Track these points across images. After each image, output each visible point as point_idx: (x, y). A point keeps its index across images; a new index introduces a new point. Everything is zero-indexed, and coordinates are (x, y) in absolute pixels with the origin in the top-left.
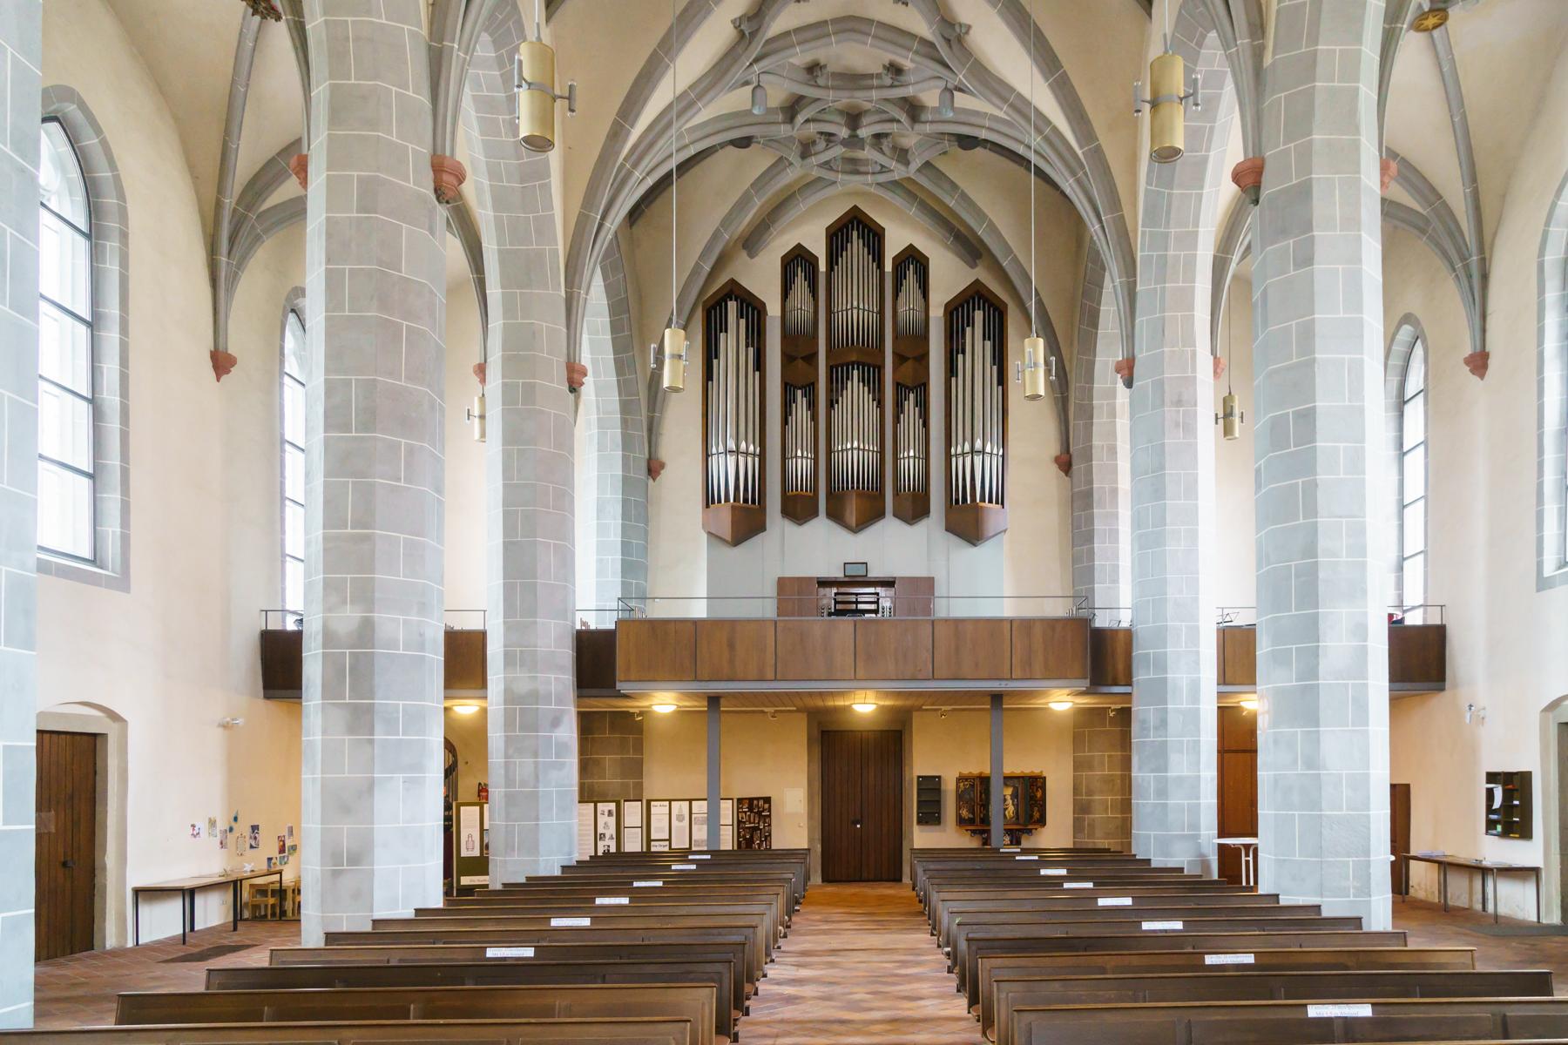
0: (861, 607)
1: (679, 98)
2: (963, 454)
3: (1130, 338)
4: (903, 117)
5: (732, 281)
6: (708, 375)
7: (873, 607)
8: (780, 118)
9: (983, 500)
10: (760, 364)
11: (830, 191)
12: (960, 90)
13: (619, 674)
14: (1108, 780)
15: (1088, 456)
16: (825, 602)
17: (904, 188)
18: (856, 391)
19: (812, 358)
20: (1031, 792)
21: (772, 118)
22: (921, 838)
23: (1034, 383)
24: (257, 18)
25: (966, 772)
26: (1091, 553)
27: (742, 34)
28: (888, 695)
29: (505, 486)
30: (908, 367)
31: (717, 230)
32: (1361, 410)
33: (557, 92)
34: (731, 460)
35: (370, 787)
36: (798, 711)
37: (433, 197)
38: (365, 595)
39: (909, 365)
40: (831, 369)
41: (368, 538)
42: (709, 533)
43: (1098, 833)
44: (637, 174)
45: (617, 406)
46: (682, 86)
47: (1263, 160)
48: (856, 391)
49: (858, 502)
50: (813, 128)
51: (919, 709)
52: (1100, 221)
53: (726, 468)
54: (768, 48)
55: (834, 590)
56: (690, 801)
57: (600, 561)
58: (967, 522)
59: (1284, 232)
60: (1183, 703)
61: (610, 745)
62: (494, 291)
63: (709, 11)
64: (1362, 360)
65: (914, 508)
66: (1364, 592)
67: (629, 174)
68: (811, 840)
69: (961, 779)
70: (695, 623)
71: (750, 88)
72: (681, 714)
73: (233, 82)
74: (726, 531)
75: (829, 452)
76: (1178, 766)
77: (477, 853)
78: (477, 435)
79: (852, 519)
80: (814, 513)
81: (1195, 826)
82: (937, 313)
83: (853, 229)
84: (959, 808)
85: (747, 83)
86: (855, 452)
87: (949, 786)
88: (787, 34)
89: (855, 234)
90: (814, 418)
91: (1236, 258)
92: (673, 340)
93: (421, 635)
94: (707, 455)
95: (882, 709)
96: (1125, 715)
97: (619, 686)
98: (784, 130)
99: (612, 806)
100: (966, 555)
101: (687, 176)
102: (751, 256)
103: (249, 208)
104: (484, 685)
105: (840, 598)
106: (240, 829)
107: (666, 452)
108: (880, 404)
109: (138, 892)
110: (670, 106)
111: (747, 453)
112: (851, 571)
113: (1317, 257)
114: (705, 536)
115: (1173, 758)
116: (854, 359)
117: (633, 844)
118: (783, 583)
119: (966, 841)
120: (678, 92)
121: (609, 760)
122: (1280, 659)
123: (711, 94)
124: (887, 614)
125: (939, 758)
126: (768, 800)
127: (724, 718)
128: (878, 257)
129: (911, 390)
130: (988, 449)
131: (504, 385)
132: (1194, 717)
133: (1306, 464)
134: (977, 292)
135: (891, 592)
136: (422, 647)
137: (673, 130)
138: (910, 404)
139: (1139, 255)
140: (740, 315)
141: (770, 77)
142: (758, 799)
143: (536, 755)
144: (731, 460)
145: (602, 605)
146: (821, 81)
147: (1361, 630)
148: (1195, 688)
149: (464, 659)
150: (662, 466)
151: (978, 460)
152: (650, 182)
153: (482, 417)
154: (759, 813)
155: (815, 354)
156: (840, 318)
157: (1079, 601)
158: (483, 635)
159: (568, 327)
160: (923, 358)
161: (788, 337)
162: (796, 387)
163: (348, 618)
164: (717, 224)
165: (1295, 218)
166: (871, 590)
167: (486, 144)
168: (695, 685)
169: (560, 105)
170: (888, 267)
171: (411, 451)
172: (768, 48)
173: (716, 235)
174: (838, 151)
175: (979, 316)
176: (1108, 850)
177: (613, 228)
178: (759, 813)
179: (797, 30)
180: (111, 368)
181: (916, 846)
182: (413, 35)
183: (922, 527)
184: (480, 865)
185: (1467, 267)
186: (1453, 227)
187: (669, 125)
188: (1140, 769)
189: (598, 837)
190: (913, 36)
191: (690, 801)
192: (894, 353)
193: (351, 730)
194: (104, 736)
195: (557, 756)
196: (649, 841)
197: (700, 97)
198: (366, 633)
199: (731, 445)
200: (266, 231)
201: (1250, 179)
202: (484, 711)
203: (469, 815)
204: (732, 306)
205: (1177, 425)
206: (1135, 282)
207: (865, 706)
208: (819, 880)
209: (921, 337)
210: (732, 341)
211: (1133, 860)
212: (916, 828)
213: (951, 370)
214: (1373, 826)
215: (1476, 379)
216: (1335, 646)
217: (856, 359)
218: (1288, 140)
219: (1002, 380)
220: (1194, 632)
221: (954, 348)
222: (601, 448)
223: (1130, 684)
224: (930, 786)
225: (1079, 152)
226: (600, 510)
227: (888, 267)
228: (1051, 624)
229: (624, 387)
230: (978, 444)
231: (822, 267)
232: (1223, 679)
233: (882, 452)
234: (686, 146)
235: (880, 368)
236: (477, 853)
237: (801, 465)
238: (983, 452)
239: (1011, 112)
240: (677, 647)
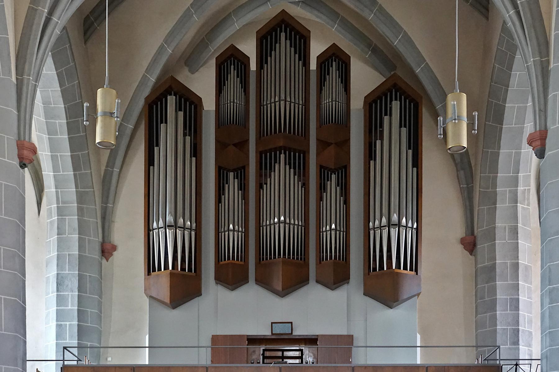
2: (381, 227)
3: (542, 112)
10: (196, 151)
15: (491, 235)
18: (282, 172)
19: (243, 144)
23: (458, 135)
30: (331, 151)
39: (332, 150)
40: (260, 154)
42: (151, 297)
45: (75, 198)
48: (282, 172)
49: (286, 269)
55: (263, 348)
57: (59, 327)
58: (385, 286)
65: (337, 277)
74: (165, 293)
75: (259, 226)
82: (357, 104)
86: (280, 223)
89: (282, 156)
90: (245, 197)
100: (384, 315)
102: (193, 72)
105: (267, 354)
107: (117, 237)
108: (305, 185)
111: (184, 228)
112: (278, 329)
114: (147, 300)
116: (281, 144)
118: (215, 339)
128: (303, 54)
129: (333, 171)
138: (332, 185)
140: (179, 108)
150: (114, 248)
151: (394, 232)
155: (247, 141)
159: (19, 110)
160: (345, 143)
161: (221, 123)
162: (230, 171)
170: (313, 66)
173: (161, 49)
175: (396, 106)
192: (318, 139)
199: (170, 219)
204: (171, 100)
206: (548, 62)
209: (343, 124)
213: (370, 154)
217: (284, 145)
219: (417, 162)
221: (373, 129)
227: (313, 66)
230: (395, 217)
231: (253, 66)
233: (306, 226)
235: (305, 153)
237: (233, 237)
238: (399, 225)
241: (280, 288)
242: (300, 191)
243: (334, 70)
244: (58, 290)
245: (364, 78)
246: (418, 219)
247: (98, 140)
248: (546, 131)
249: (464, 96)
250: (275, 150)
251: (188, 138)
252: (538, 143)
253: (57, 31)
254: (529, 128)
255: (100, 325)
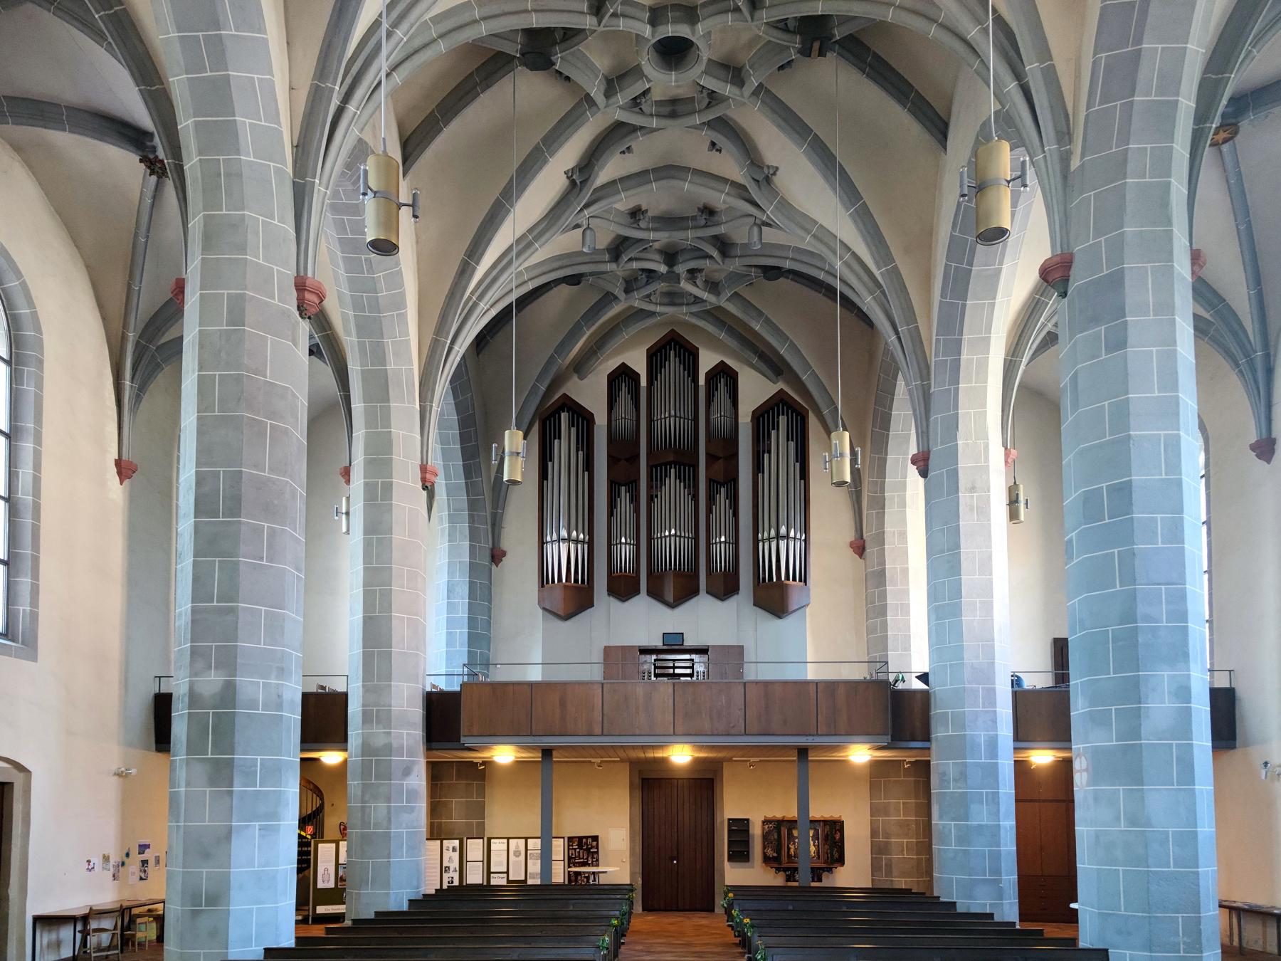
0: (677, 671)
1: (518, 241)
2: (769, 539)
4: (715, 254)
5: (565, 395)
6: (543, 475)
7: (688, 671)
8: (607, 257)
9: (794, 579)
10: (589, 465)
11: (650, 322)
12: (768, 225)
13: (464, 730)
14: (904, 825)
15: (880, 539)
16: (646, 667)
17: (716, 316)
18: (672, 485)
20: (832, 833)
21: (598, 258)
22: (733, 875)
24: (154, 178)
25: (770, 815)
26: (884, 625)
27: (573, 183)
28: (701, 748)
29: (365, 569)
31: (552, 357)
32: (1179, 483)
33: (402, 200)
34: (564, 547)
35: (228, 835)
36: (622, 761)
37: (297, 313)
38: (228, 661)
40: (651, 468)
41: (233, 611)
42: (544, 609)
43: (895, 873)
44: (482, 306)
45: (466, 505)
46: (520, 231)
47: (1072, 255)
48: (672, 485)
49: (677, 585)
50: (635, 265)
51: (730, 760)
52: (897, 333)
53: (561, 554)
54: (597, 195)
55: (654, 657)
56: (526, 839)
57: (449, 634)
58: (774, 598)
59: (1095, 320)
60: (985, 759)
61: (456, 784)
62: (357, 405)
63: (545, 162)
64: (1178, 436)
65: (725, 587)
66: (1186, 656)
67: (475, 305)
68: (632, 874)
69: (765, 822)
70: (532, 685)
71: (580, 231)
72: (519, 764)
73: (136, 235)
76: (980, 816)
77: (331, 885)
78: (344, 530)
79: (670, 597)
80: (636, 592)
81: (997, 871)
82: (745, 418)
83: (673, 350)
84: (764, 847)
85: (577, 226)
86: (672, 540)
87: (756, 830)
88: (613, 183)
91: (1025, 361)
92: (513, 440)
93: (279, 696)
94: (542, 543)
95: (697, 761)
96: (923, 769)
97: (463, 740)
98: (610, 267)
99: (456, 843)
101: (527, 311)
103: (150, 341)
104: (345, 740)
105: (659, 664)
106: (136, 857)
107: (506, 544)
108: (695, 498)
109: (38, 920)
110: (510, 249)
113: (1130, 340)
114: (541, 611)
115: (974, 808)
116: (671, 459)
117: (475, 876)
118: (607, 650)
119: (776, 880)
120: (518, 235)
121: (456, 803)
122: (1099, 720)
123: (548, 235)
124: (701, 677)
125: (749, 802)
126: (595, 838)
127: (555, 766)
129: (722, 484)
130: (792, 534)
131: (366, 484)
132: (992, 771)
133: (1124, 533)
134: (782, 400)
135: (704, 658)
136: (280, 706)
137: (512, 269)
139: (933, 361)
140: (571, 424)
141: (598, 220)
142: (587, 837)
143: (389, 800)
144: (564, 547)
145: (451, 670)
146: (642, 224)
147: (1184, 693)
148: (993, 744)
149: (323, 717)
150: (504, 554)
151: (783, 544)
152: (493, 313)
153: (347, 514)
154: (588, 850)
155: (638, 456)
156: (659, 426)
157: (884, 669)
158: (345, 696)
159: (422, 435)
163: (212, 681)
164: (551, 351)
165: (1108, 306)
166: (687, 657)
167: (351, 281)
168: (530, 739)
169: (405, 213)
170: (702, 381)
171: (273, 533)
172: (597, 195)
173: (551, 360)
174: (661, 286)
175: (783, 420)
176: (908, 891)
177: (462, 351)
178: (588, 850)
179: (622, 179)
180: (25, 472)
181: (727, 883)
182: (277, 170)
183: (732, 602)
184: (335, 895)
185: (1251, 363)
186: (1236, 327)
187: (510, 263)
188: (941, 818)
189: (443, 870)
190: (725, 180)
191: (526, 839)
192: (707, 454)
193: (213, 781)
194: (12, 784)
195: (408, 802)
196: (489, 873)
197: (536, 238)
198: (228, 694)
199: (564, 533)
200: (164, 361)
201: (1055, 275)
202: (345, 762)
203: (325, 852)
205: (972, 509)
206: (929, 385)
207: (681, 755)
208: (640, 909)
210: (564, 447)
211: (935, 901)
212: (727, 864)
213: (758, 467)
214: (1202, 883)
215: (1263, 463)
216: (1159, 707)
218: (1098, 233)
219: (804, 475)
220: (991, 694)
222: (451, 538)
223: (928, 739)
224: (740, 828)
225: (877, 273)
226: (450, 591)
227: (702, 381)
228: (852, 686)
229: (471, 488)
230: (783, 530)
231: (643, 382)
232: (1017, 738)
233: (696, 538)
234: (525, 282)
235: (695, 467)
236: (331, 885)
237: (625, 552)
238: (787, 537)
239: (814, 242)
240: (517, 709)
241: (671, 600)
242: (691, 504)
243: (722, 386)
244: (448, 598)
245: (754, 390)
246: (806, 530)
247: (505, 478)
248: (929, 452)
249: (847, 434)
250: (666, 465)
251: (580, 453)
252: (922, 463)
253: (458, 359)
254: (913, 450)
255: (489, 631)
